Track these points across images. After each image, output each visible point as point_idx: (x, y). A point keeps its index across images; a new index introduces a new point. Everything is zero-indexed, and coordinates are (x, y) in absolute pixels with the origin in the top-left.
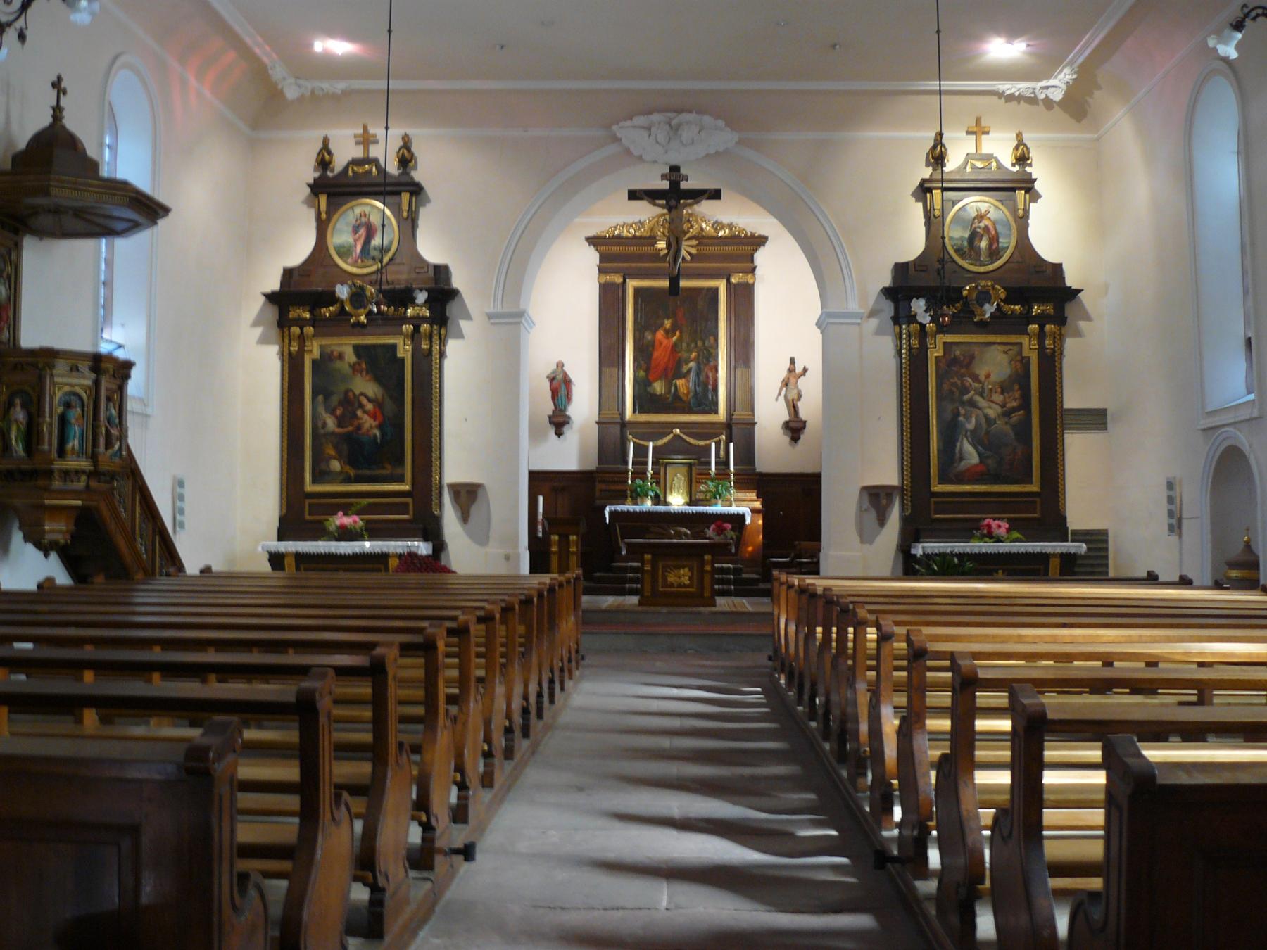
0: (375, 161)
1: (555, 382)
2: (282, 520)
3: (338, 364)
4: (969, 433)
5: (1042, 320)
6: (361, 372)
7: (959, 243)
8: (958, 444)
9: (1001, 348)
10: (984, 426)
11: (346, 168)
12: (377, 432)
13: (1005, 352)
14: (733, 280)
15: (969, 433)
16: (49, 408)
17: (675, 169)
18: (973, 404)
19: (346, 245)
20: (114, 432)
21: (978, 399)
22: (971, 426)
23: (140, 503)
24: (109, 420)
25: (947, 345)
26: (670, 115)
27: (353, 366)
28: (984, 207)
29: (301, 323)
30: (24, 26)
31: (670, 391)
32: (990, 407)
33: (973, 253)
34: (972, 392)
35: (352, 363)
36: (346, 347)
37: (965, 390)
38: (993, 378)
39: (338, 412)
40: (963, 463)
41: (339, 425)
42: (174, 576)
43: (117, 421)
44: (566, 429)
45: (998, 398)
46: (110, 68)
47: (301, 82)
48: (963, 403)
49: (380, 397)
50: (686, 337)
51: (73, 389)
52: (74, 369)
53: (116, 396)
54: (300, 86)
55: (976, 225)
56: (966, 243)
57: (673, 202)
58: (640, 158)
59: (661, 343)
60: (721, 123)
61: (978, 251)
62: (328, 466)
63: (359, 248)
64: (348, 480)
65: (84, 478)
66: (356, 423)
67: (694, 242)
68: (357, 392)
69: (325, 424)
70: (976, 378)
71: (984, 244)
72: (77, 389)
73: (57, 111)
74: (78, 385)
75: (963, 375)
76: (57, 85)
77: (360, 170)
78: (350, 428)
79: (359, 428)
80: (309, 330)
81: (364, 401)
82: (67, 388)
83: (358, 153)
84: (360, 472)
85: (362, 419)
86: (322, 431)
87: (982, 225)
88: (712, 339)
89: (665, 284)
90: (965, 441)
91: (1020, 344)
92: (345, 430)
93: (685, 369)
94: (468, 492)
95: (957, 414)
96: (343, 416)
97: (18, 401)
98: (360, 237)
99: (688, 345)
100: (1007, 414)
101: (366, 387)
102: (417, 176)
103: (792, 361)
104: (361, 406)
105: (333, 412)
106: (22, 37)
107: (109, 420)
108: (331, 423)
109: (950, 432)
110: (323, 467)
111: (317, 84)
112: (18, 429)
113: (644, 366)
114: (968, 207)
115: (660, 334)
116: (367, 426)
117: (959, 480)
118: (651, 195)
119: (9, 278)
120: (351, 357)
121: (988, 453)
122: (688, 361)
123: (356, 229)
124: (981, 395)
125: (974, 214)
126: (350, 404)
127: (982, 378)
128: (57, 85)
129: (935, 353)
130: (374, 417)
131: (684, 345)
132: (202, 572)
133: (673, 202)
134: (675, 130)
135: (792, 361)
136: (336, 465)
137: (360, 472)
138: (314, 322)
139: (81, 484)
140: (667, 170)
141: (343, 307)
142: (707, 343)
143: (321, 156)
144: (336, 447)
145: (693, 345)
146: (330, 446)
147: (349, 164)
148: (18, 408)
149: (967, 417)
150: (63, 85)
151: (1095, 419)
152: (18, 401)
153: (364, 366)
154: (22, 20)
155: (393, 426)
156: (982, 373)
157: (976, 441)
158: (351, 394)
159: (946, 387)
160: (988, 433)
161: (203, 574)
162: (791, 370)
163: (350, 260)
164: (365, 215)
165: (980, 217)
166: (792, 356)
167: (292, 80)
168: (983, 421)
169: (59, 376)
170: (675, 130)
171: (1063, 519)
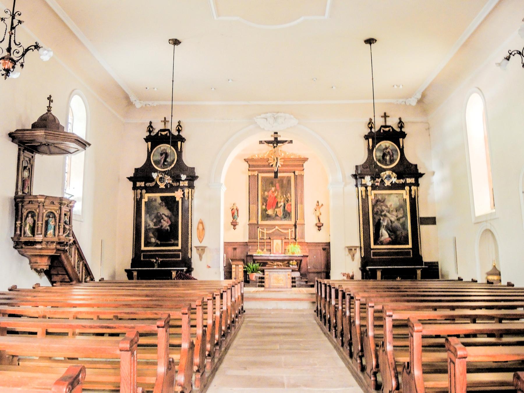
0: (168, 130)
1: (233, 210)
2: (133, 260)
3: (154, 203)
4: (384, 227)
5: (410, 185)
6: (163, 206)
7: (379, 158)
8: (381, 231)
9: (396, 195)
10: (390, 224)
11: (158, 133)
12: (169, 228)
13: (397, 197)
14: (296, 174)
15: (384, 227)
16: (158, 252)
17: (276, 133)
18: (385, 215)
19: (158, 160)
20: (67, 227)
21: (387, 214)
22: (385, 224)
23: (78, 254)
24: (65, 223)
25: (375, 195)
26: (275, 114)
27: (160, 204)
28: (387, 145)
29: (141, 188)
30: (23, 62)
31: (274, 213)
32: (392, 217)
33: (384, 161)
34: (385, 212)
35: (159, 203)
36: (157, 195)
37: (383, 211)
38: (393, 206)
39: (155, 220)
40: (382, 238)
41: (155, 225)
42: (89, 282)
43: (68, 223)
44: (237, 227)
45: (395, 213)
46: (71, 94)
47: (142, 102)
48: (382, 215)
49: (170, 215)
50: (280, 194)
51: (51, 211)
52: (53, 203)
53: (69, 214)
54: (141, 103)
55: (385, 151)
56: (381, 158)
57: (275, 145)
58: (264, 129)
59: (271, 196)
60: (292, 116)
61: (386, 161)
62: (150, 240)
63: (162, 161)
64: (157, 245)
65: (55, 244)
66: (161, 224)
67: (283, 160)
68: (161, 214)
69: (149, 225)
70: (387, 206)
71: (388, 158)
72: (53, 211)
73: (49, 108)
74: (54, 209)
75: (381, 206)
76: (49, 98)
77: (163, 133)
78: (159, 227)
79: (162, 226)
80: (144, 191)
81: (164, 216)
82: (49, 211)
83: (163, 127)
84: (162, 242)
85: (163, 223)
86: (148, 228)
87: (387, 151)
88: (289, 194)
89: (272, 175)
90: (383, 229)
91: (403, 194)
92: (157, 227)
93: (279, 205)
94: (202, 250)
95: (380, 219)
96: (156, 222)
97: (30, 215)
98: (163, 158)
99: (280, 197)
100: (398, 219)
101: (165, 211)
102: (182, 134)
103: (318, 202)
104: (163, 218)
105: (152, 221)
106: (22, 65)
107: (65, 223)
108: (152, 225)
109: (378, 226)
110: (149, 241)
111: (147, 103)
112: (30, 226)
113: (265, 204)
114: (382, 145)
115: (270, 192)
116: (164, 226)
117: (382, 243)
118: (269, 142)
119: (29, 169)
120: (159, 201)
121: (392, 233)
122: (280, 202)
123: (161, 154)
124: (389, 212)
125: (384, 147)
126: (159, 219)
127: (389, 206)
128: (49, 98)
129: (371, 198)
130: (168, 222)
131: (279, 197)
132: (100, 280)
133: (275, 145)
134: (275, 119)
135: (318, 202)
136: (153, 240)
137: (162, 242)
138: (145, 188)
139: (54, 246)
140: (273, 134)
141: (156, 182)
142: (287, 196)
143: (148, 129)
144: (153, 234)
145: (282, 197)
146: (151, 233)
147: (159, 131)
148: (30, 218)
149: (383, 220)
150: (52, 99)
151: (432, 221)
152: (30, 215)
153: (164, 204)
154: (22, 60)
155: (174, 226)
156: (389, 205)
157: (387, 228)
158: (159, 214)
159: (375, 210)
160: (391, 226)
161: (11, 292)
162: (318, 205)
163: (159, 166)
164: (165, 150)
165: (386, 148)
166: (318, 200)
167: (138, 101)
168: (390, 222)
169: (46, 206)
170: (275, 119)
171: (421, 258)
